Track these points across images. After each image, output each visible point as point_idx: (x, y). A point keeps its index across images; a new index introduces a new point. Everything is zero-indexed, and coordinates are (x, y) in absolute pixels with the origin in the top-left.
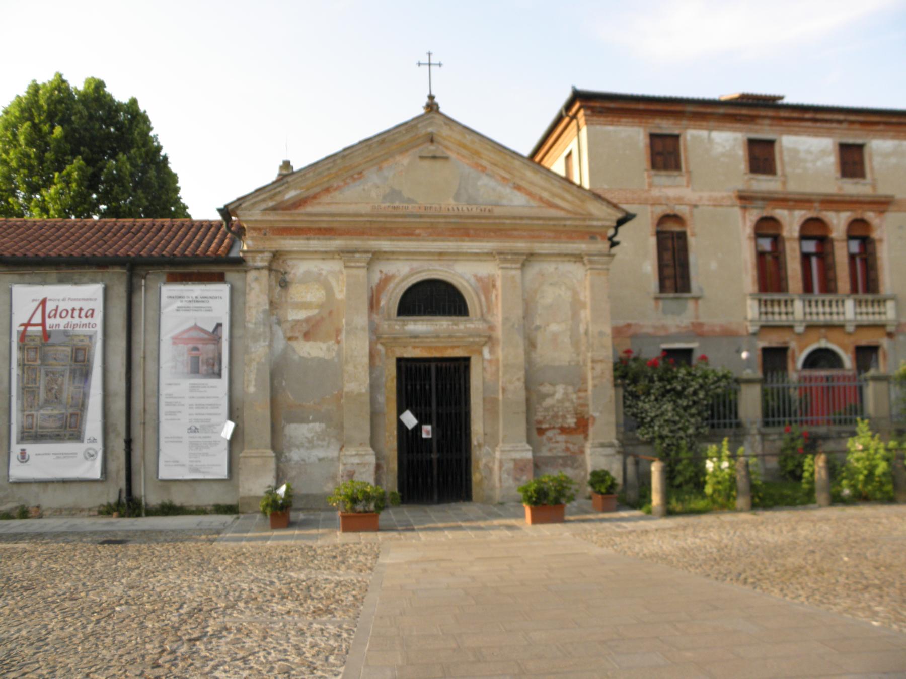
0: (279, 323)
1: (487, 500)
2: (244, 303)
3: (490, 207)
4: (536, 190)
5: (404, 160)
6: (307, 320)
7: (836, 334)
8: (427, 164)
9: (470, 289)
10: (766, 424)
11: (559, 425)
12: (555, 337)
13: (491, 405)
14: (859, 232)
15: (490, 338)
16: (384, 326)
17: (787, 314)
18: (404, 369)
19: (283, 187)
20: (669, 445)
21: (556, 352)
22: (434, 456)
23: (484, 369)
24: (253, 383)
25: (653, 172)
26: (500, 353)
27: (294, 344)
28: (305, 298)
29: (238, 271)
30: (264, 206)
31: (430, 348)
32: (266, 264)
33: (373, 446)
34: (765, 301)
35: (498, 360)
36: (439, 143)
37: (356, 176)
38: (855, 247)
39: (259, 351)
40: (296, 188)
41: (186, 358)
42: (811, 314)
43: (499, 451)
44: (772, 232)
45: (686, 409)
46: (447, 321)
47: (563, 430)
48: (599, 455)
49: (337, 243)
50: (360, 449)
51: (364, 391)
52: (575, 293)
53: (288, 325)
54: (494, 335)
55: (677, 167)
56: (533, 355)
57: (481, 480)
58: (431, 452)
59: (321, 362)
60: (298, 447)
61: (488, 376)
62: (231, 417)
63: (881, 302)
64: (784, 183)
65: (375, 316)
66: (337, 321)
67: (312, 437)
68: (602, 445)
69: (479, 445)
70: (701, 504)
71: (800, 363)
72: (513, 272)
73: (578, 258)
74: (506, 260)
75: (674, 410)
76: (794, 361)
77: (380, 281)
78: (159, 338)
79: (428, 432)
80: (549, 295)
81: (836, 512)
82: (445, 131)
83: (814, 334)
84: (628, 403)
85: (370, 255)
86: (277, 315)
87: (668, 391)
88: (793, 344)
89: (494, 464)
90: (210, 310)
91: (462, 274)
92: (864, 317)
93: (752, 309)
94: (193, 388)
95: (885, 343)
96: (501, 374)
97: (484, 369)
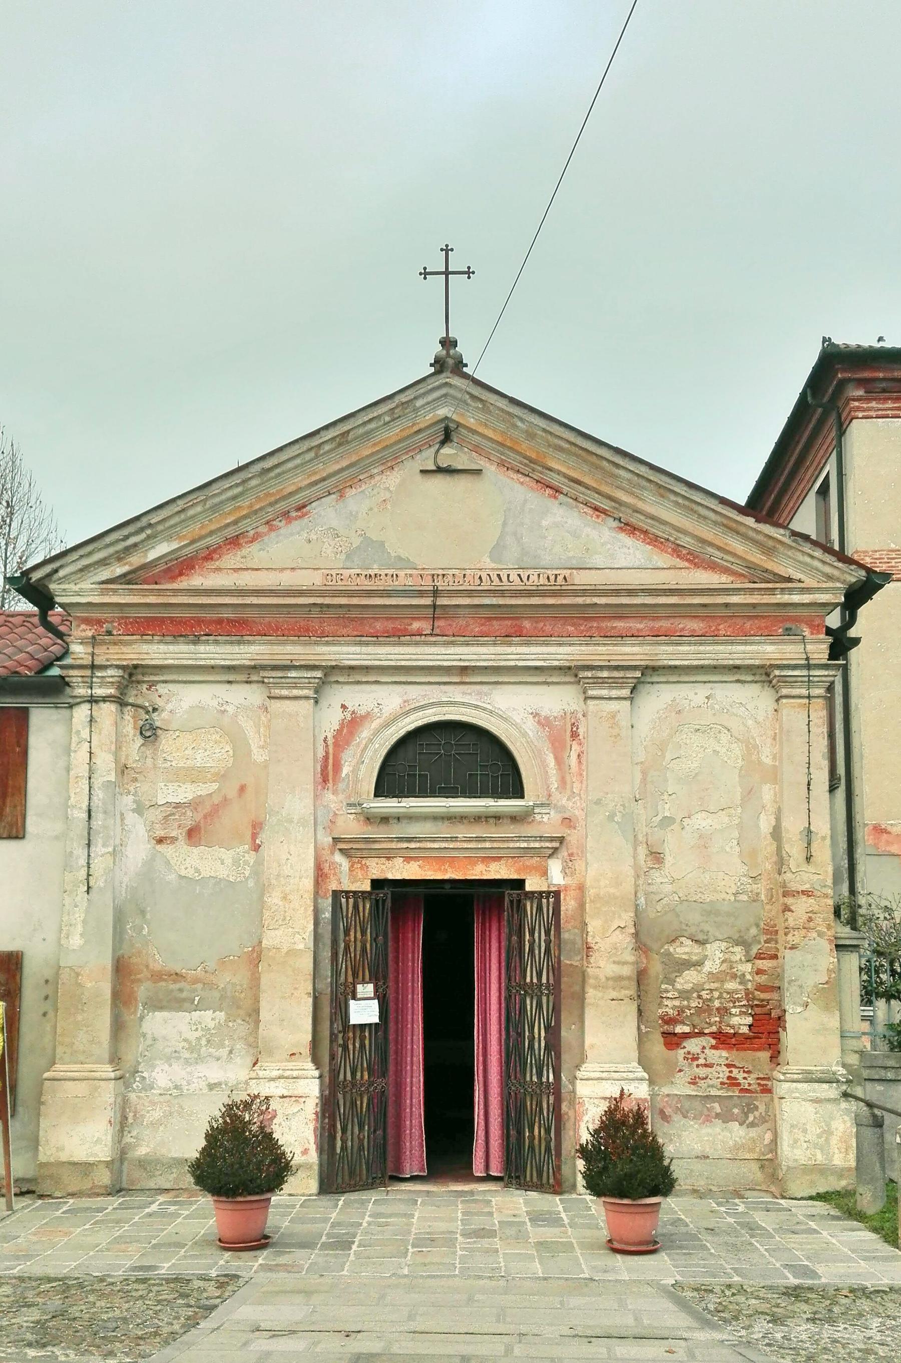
3: (567, 573)
6: (194, 804)
8: (439, 483)
11: (714, 1029)
19: (143, 536)
24: (80, 928)
37: (294, 514)
40: (169, 539)
47: (723, 1039)
50: (290, 1065)
51: (301, 946)
60: (168, 1059)
67: (198, 1039)
72: (614, 706)
73: (765, 674)
77: (342, 725)
85: (319, 674)
91: (512, 713)
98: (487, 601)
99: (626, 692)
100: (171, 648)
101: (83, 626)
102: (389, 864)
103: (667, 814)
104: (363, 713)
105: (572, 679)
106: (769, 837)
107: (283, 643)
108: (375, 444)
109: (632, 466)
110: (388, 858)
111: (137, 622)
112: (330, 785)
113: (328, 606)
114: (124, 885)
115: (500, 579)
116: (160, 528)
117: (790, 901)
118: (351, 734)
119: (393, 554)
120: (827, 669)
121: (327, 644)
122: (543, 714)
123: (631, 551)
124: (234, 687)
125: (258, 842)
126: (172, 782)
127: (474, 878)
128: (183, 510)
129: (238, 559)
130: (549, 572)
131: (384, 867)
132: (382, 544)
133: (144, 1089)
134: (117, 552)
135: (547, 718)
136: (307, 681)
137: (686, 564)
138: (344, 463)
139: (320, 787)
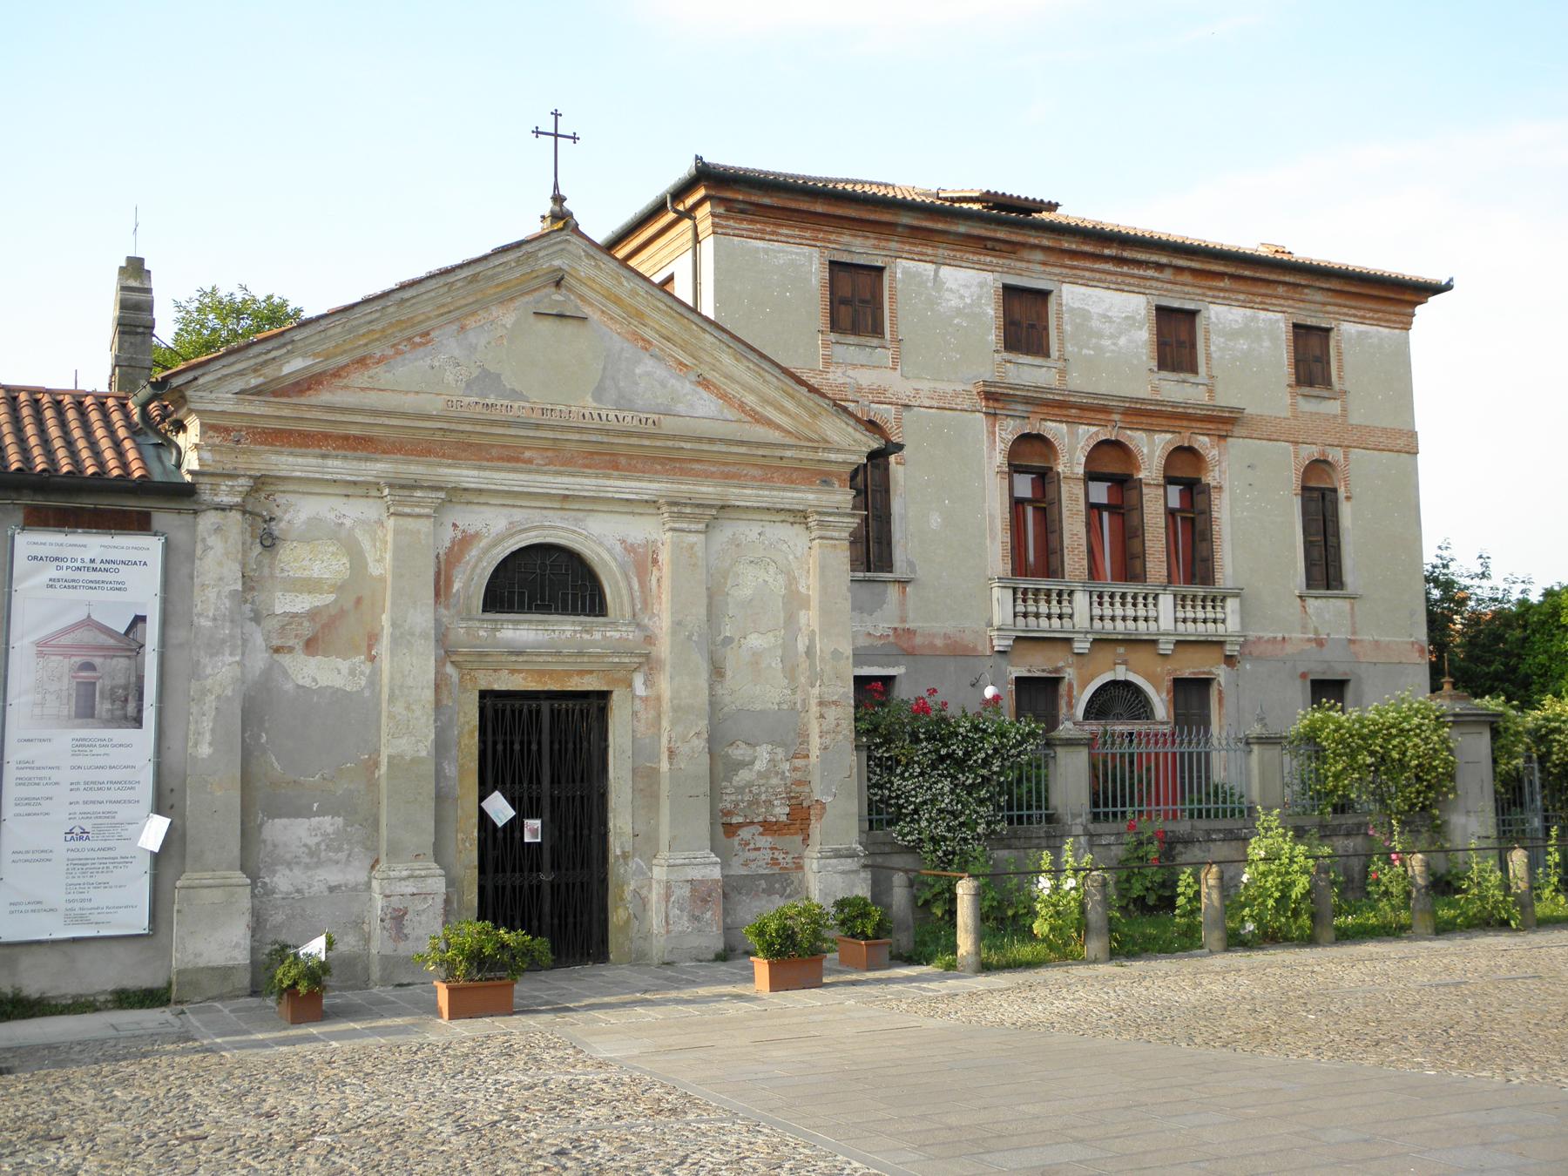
0: (257, 618)
1: (638, 960)
3: (655, 417)
4: (733, 389)
5: (508, 317)
6: (313, 614)
7: (1142, 656)
8: (546, 325)
9: (613, 564)
10: (1096, 817)
11: (761, 819)
12: (756, 655)
13: (646, 778)
14: (1187, 473)
15: (647, 656)
16: (460, 631)
17: (1060, 617)
18: (490, 713)
19: (284, 350)
20: (946, 853)
21: (759, 689)
22: (546, 877)
23: (635, 714)
24: (208, 737)
25: (833, 337)
26: (665, 686)
27: (285, 659)
28: (311, 568)
29: (179, 511)
30: (240, 384)
31: (542, 673)
32: (238, 499)
33: (438, 858)
34: (1025, 591)
35: (659, 699)
37: (417, 340)
38: (1175, 496)
39: (221, 674)
40: (304, 355)
41: (66, 685)
42: (1102, 618)
43: (658, 867)
44: (1037, 463)
45: (970, 790)
47: (769, 827)
48: (828, 876)
49: (378, 468)
50: (416, 865)
51: (424, 754)
52: (792, 580)
53: (273, 624)
55: (877, 330)
57: (628, 921)
58: (539, 870)
59: (338, 695)
60: (289, 865)
61: (641, 728)
62: (160, 805)
63: (1217, 600)
64: (1063, 373)
66: (370, 616)
67: (318, 844)
68: (837, 854)
69: (625, 856)
70: (1025, 951)
71: (1079, 712)
72: (693, 538)
73: (799, 516)
74: (680, 516)
75: (952, 792)
76: (1070, 706)
77: (453, 542)
78: (7, 643)
79: (534, 833)
80: (749, 582)
81: (1238, 958)
83: (1106, 655)
84: (875, 779)
85: (442, 495)
86: (253, 602)
87: (942, 759)
88: (1069, 674)
89: (650, 890)
90: (120, 587)
91: (600, 538)
92: (1190, 626)
93: (1001, 606)
94: (80, 747)
95: (1221, 673)
96: (665, 724)
97: (635, 714)
98: (593, 438)
99: (701, 526)
100: (300, 460)
107: (409, 462)
112: (442, 599)
117: (824, 710)
118: (462, 552)
124: (351, 500)
132: (499, 376)
133: (266, 894)
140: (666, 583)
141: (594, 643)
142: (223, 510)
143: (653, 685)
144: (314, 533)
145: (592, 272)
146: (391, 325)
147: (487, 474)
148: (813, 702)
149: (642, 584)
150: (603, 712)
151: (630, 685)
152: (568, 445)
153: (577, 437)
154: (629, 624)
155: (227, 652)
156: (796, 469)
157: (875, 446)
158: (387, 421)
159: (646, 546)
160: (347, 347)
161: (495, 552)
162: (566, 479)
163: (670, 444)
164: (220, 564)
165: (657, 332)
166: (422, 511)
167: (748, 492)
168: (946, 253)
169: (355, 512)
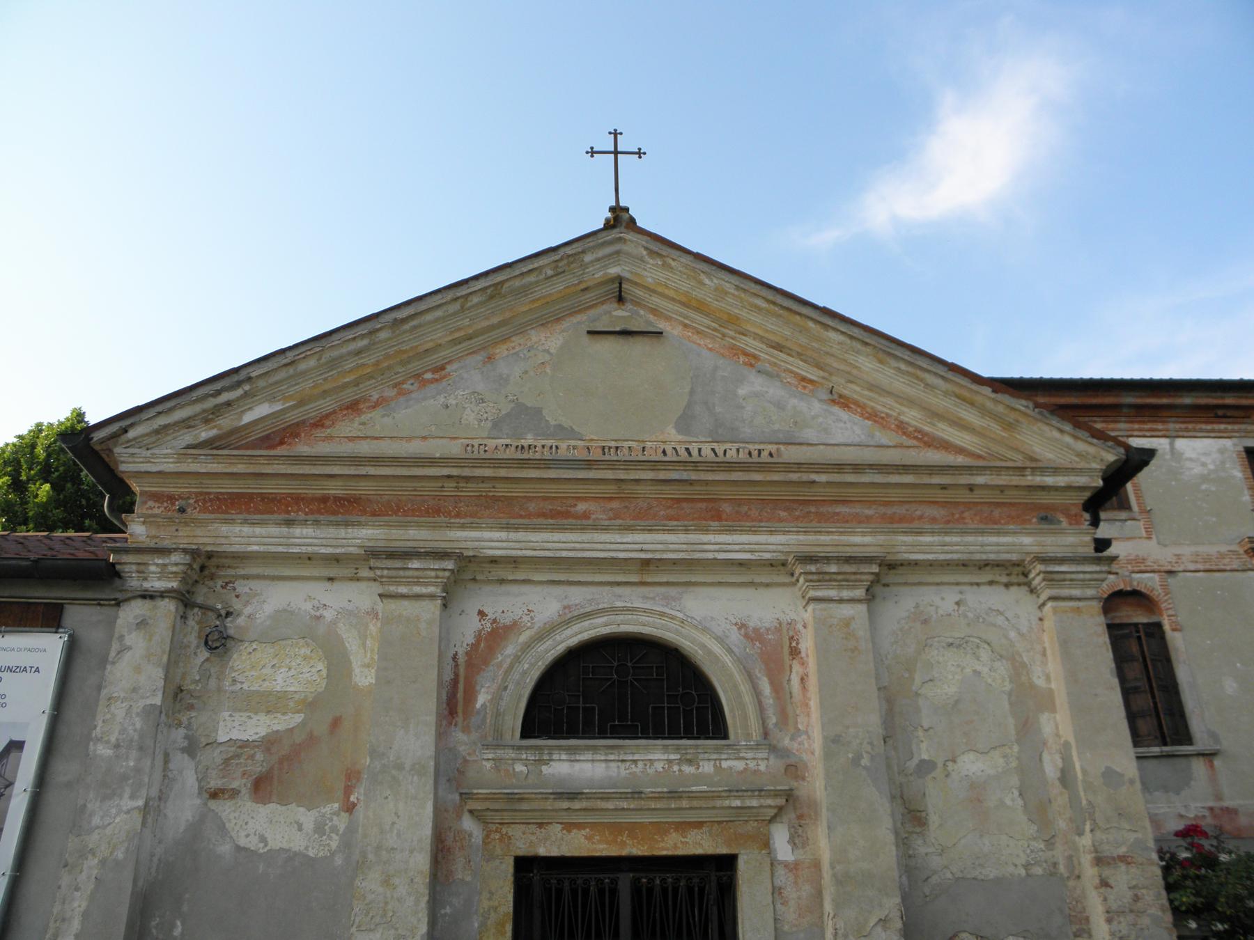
0: (191, 749)
2: (99, 688)
3: (773, 448)
4: (883, 405)
5: (552, 340)
6: (269, 743)
9: (727, 660)
12: (977, 791)
15: (789, 796)
16: (484, 764)
19: (239, 392)
23: (776, 891)
26: (823, 844)
27: (224, 809)
29: (99, 603)
30: (188, 438)
31: (616, 828)
35: (817, 865)
36: (637, 303)
37: (428, 376)
40: (272, 399)
46: (665, 749)
52: (1019, 669)
53: (216, 756)
54: (802, 790)
56: (920, 847)
61: (790, 914)
65: (460, 739)
72: (847, 610)
73: (1013, 572)
74: (823, 579)
77: (478, 638)
80: (948, 676)
82: (651, 273)
85: (450, 565)
86: (188, 727)
91: (707, 622)
96: (828, 907)
97: (776, 891)
98: (674, 475)
100: (258, 530)
101: (151, 503)
102: (541, 833)
103: (925, 756)
104: (508, 621)
105: (787, 579)
106: (1057, 783)
108: (533, 301)
109: (843, 327)
110: (540, 825)
111: (218, 499)
112: (460, 719)
113: (467, 479)
114: (155, 859)
115: (690, 454)
116: (261, 383)
117: (1107, 872)
119: (553, 423)
120: (1098, 564)
121: (463, 527)
122: (751, 624)
123: (849, 425)
124: (336, 585)
125: (353, 798)
126: (240, 711)
127: (664, 853)
128: (293, 362)
129: (356, 425)
130: (751, 447)
131: (533, 838)
132: (538, 411)
134: (204, 411)
135: (756, 630)
136: (433, 574)
137: (915, 443)
138: (495, 320)
139: (444, 723)
140: (813, 682)
141: (699, 779)
142: (152, 597)
143: (805, 844)
144: (281, 632)
145: (661, 275)
146: (388, 357)
147: (521, 535)
148: (1086, 860)
149: (777, 688)
150: (727, 890)
151: (766, 844)
152: (640, 489)
153: (649, 475)
154: (757, 747)
155: (128, 791)
156: (998, 504)
157: (1111, 457)
158: (372, 471)
159: (778, 629)
160: (327, 386)
161: (542, 648)
162: (639, 537)
163: (794, 477)
164: (138, 669)
165: (762, 339)
166: (424, 590)
167: (927, 539)
168: (1178, 426)
169: (346, 602)
